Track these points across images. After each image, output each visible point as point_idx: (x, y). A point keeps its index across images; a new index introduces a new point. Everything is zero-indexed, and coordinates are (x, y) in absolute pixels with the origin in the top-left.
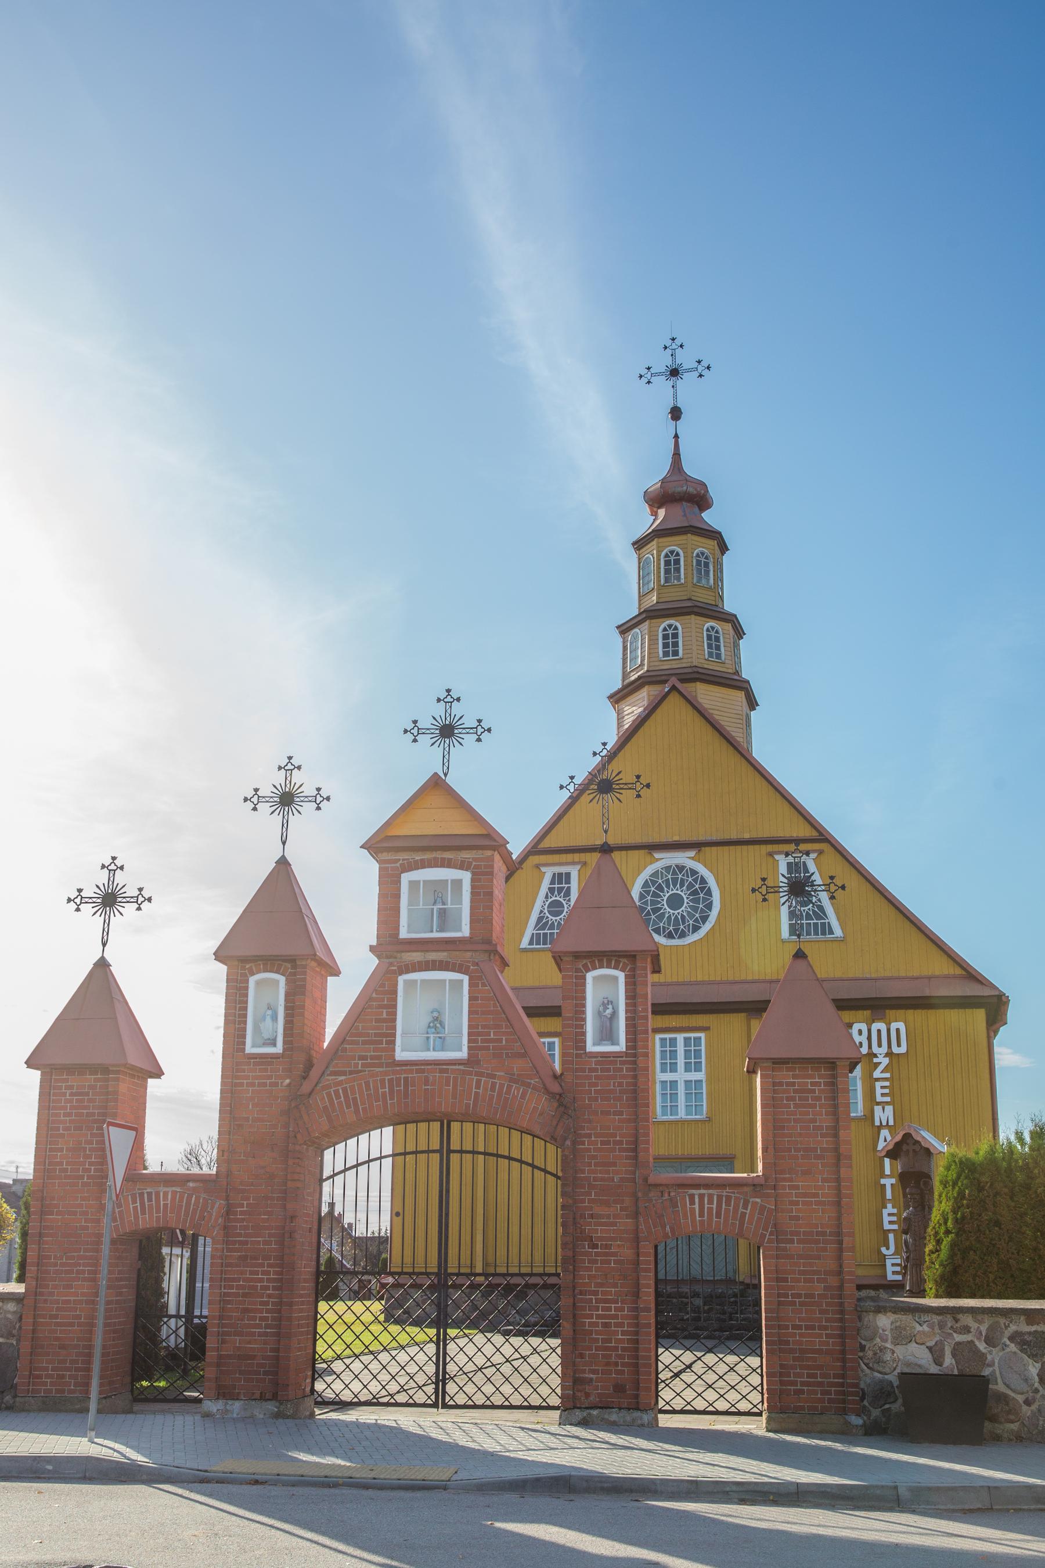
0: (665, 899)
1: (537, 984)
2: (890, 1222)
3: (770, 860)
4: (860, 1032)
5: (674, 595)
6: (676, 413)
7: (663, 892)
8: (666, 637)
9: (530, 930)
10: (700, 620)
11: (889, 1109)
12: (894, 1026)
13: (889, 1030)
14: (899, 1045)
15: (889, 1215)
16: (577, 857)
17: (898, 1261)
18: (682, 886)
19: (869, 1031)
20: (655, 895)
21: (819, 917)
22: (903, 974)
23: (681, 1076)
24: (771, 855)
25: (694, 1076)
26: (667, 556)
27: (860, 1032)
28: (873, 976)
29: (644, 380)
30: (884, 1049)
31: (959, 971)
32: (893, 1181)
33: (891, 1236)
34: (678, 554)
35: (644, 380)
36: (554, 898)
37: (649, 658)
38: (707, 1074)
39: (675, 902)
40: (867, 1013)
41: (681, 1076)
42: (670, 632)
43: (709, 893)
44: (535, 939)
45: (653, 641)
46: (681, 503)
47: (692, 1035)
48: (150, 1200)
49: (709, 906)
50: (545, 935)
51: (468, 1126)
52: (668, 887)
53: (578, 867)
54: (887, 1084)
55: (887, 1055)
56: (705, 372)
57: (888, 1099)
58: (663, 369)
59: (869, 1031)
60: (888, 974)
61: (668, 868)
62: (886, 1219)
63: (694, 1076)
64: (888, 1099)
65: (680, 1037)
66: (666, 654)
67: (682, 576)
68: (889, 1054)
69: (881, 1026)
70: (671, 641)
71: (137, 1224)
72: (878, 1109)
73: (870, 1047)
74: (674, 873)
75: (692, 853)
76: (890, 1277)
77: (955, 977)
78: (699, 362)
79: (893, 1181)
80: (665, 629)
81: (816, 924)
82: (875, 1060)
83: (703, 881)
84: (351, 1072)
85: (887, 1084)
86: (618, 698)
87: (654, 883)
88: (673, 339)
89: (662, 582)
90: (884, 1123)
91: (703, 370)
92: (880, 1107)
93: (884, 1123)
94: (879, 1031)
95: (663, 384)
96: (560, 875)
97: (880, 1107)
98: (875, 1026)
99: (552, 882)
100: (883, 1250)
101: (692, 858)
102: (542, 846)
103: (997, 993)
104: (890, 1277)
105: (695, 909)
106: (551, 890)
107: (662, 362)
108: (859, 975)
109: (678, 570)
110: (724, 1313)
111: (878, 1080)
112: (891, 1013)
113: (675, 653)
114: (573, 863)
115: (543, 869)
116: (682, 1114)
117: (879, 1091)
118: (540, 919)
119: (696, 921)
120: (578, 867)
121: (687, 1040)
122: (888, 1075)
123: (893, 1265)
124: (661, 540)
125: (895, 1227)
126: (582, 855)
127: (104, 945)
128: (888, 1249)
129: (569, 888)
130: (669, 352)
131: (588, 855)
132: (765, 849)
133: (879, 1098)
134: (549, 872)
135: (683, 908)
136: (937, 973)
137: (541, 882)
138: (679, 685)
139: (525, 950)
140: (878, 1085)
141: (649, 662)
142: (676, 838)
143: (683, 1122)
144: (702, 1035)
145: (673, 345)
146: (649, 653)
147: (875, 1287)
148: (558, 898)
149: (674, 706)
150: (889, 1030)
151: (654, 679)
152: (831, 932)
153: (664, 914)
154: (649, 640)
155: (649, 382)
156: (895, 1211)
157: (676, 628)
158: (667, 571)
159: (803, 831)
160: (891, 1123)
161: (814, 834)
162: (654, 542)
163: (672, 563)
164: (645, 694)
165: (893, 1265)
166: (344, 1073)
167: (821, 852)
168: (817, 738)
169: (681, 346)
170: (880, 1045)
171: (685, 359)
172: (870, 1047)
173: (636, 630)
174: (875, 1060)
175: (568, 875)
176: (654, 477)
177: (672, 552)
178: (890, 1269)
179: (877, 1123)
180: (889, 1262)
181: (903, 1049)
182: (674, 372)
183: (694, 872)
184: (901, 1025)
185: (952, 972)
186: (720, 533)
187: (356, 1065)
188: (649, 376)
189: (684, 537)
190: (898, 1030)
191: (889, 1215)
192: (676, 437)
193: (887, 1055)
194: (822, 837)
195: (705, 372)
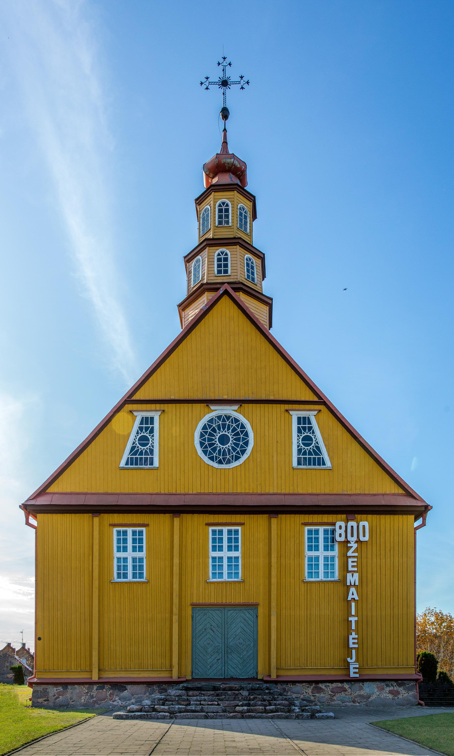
0: (217, 437)
1: (131, 491)
2: (354, 643)
3: (287, 414)
4: (340, 527)
6: (225, 114)
7: (216, 432)
8: (219, 260)
9: (126, 455)
11: (356, 575)
12: (361, 524)
13: (358, 527)
14: (364, 536)
15: (353, 639)
16: (158, 406)
17: (357, 666)
18: (220, 450)
19: (346, 527)
20: (210, 434)
21: (316, 454)
22: (367, 492)
23: (225, 554)
25: (233, 554)
26: (220, 206)
27: (340, 527)
28: (349, 493)
29: (204, 86)
30: (355, 538)
31: (401, 491)
32: (356, 619)
33: (354, 651)
34: (227, 205)
35: (204, 86)
36: (142, 434)
37: (208, 274)
38: (242, 553)
39: (224, 440)
40: (344, 516)
41: (225, 554)
43: (247, 434)
45: (210, 263)
47: (233, 528)
49: (247, 444)
50: (136, 459)
52: (219, 429)
53: (160, 413)
54: (356, 560)
55: (356, 542)
56: (245, 86)
57: (355, 569)
58: (217, 80)
59: (346, 527)
60: (358, 492)
61: (219, 417)
62: (351, 641)
63: (233, 554)
64: (355, 569)
65: (225, 529)
66: (219, 272)
67: (230, 221)
68: (358, 541)
69: (354, 524)
70: (223, 263)
72: (349, 575)
73: (346, 537)
75: (236, 407)
76: (352, 675)
77: (399, 495)
78: (242, 77)
79: (356, 619)
80: (219, 255)
81: (314, 459)
82: (349, 545)
83: (243, 427)
85: (356, 560)
86: (184, 306)
87: (210, 426)
88: (224, 58)
89: (217, 224)
90: (353, 584)
91: (243, 83)
92: (351, 574)
93: (353, 584)
94: (352, 527)
95: (216, 90)
96: (147, 418)
97: (351, 574)
98: (351, 523)
99: (141, 423)
100: (349, 659)
101: (235, 411)
102: (134, 398)
103: (424, 504)
104: (352, 675)
105: (234, 449)
106: (141, 429)
107: (216, 75)
108: (340, 492)
109: (227, 216)
110: (264, 700)
111: (350, 557)
112: (358, 517)
113: (226, 272)
114: (156, 411)
115: (135, 414)
116: (225, 578)
117: (350, 564)
118: (133, 448)
120: (160, 413)
121: (230, 532)
122: (356, 554)
123: (354, 668)
124: (217, 194)
125: (356, 646)
126: (162, 405)
128: (351, 659)
129: (153, 428)
130: (221, 67)
131: (166, 405)
133: (350, 569)
134: (139, 416)
135: (229, 444)
136: (388, 492)
137: (134, 422)
139: (123, 469)
140: (350, 560)
141: (208, 277)
143: (226, 582)
144: (239, 528)
145: (224, 63)
146: (208, 271)
147: (342, 681)
148: (145, 434)
149: (225, 299)
150: (358, 527)
152: (324, 464)
153: (216, 447)
154: (208, 262)
155: (207, 88)
156: (357, 636)
157: (226, 254)
158: (220, 217)
160: (357, 583)
162: (212, 196)
163: (223, 212)
164: (205, 298)
165: (354, 668)
168: (329, 322)
169: (230, 64)
170: (352, 536)
171: (233, 74)
172: (346, 537)
173: (199, 257)
174: (349, 545)
175: (152, 419)
177: (223, 203)
178: (352, 670)
179: (348, 584)
180: (351, 667)
181: (367, 538)
182: (225, 83)
183: (237, 420)
184: (366, 524)
185: (397, 492)
186: (254, 197)
189: (232, 193)
190: (364, 526)
191: (353, 639)
192: (225, 130)
193: (356, 542)
194: (321, 401)
195: (245, 86)
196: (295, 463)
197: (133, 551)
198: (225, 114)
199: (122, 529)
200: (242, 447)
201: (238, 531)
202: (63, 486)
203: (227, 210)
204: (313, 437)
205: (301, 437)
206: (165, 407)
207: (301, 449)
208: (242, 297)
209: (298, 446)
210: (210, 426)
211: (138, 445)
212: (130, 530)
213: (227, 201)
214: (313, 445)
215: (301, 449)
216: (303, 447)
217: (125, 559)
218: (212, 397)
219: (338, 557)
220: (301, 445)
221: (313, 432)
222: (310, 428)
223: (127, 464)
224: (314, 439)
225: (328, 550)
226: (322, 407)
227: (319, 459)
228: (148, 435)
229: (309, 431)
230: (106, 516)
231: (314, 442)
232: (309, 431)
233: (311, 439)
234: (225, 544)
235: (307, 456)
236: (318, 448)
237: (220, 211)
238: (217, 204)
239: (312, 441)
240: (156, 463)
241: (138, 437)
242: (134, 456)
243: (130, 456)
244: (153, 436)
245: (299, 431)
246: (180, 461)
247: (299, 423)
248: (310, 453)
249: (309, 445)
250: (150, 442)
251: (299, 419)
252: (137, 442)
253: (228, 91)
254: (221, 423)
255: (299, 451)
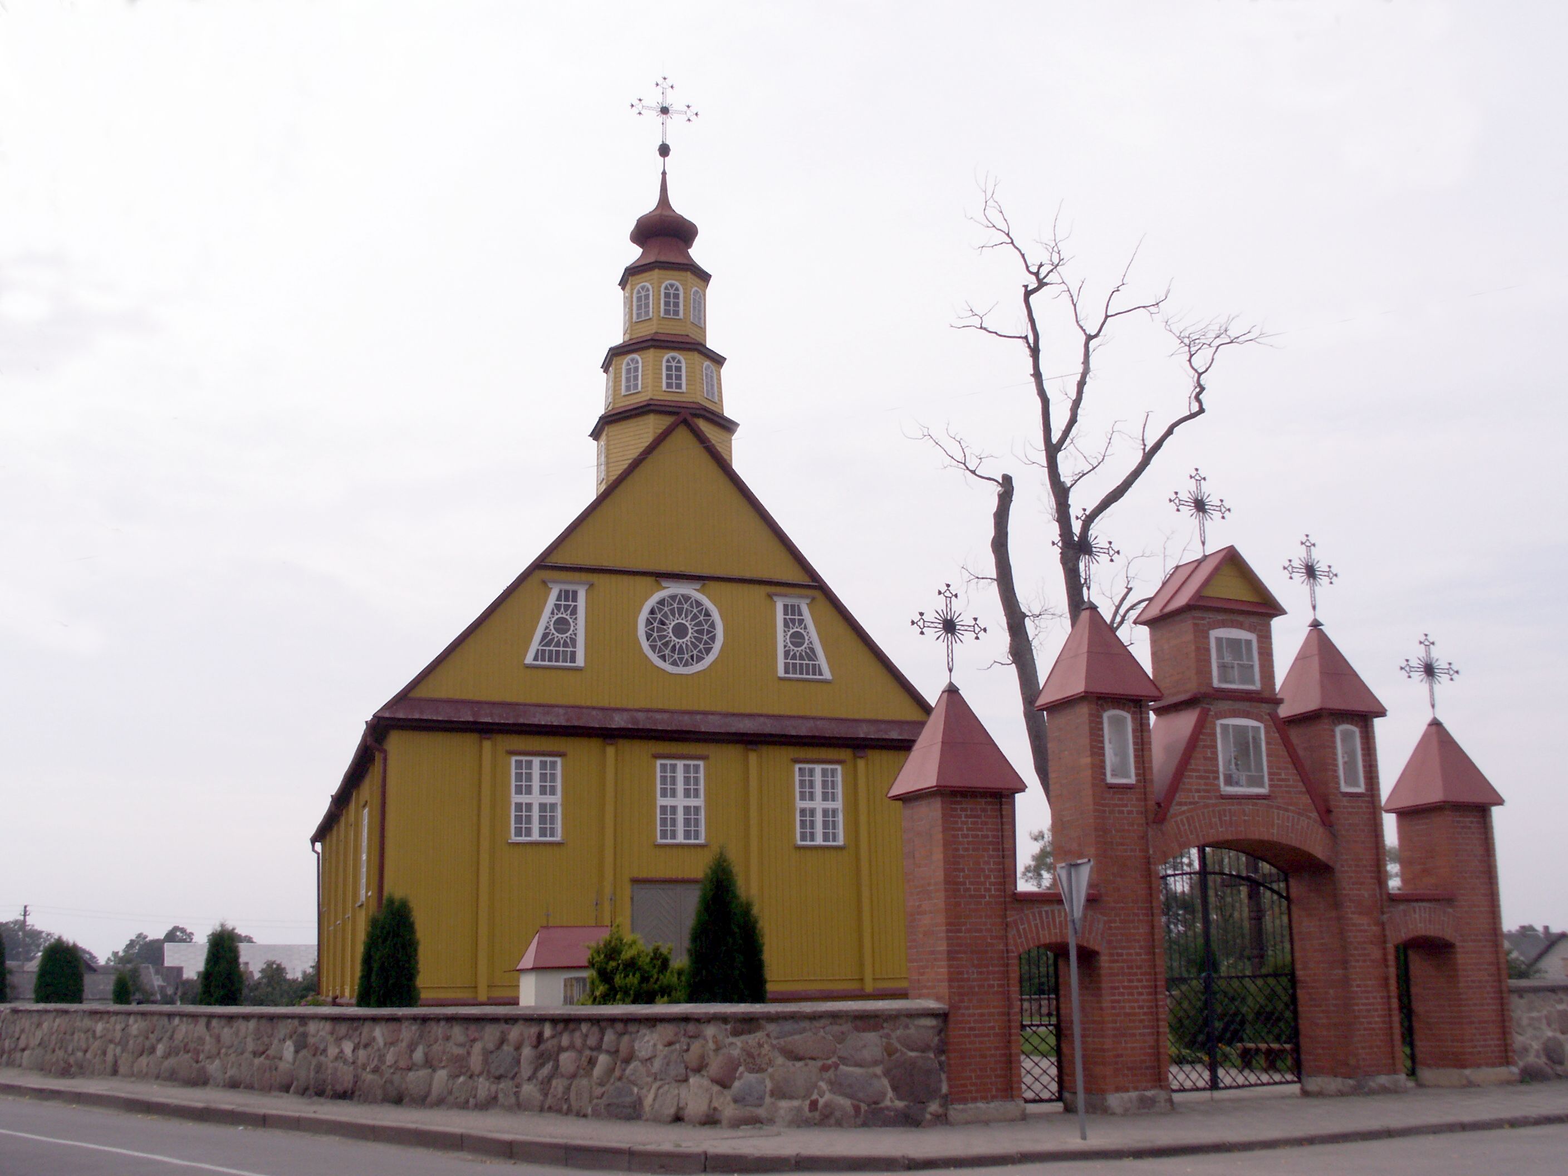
5: (646, 331)
6: (664, 150)
9: (535, 645)
10: (659, 352)
16: (584, 576)
23: (680, 802)
24: (770, 596)
36: (560, 615)
38: (705, 801)
39: (680, 631)
41: (680, 802)
42: (674, 364)
44: (539, 655)
46: (664, 238)
48: (1047, 917)
50: (551, 651)
51: (1232, 853)
70: (674, 373)
71: (1039, 939)
74: (680, 603)
84: (1191, 803)
89: (662, 314)
96: (567, 592)
99: (559, 599)
106: (558, 607)
113: (679, 386)
118: (545, 636)
119: (700, 651)
127: (951, 670)
130: (659, 89)
132: (762, 590)
138: (689, 418)
142: (682, 569)
149: (682, 437)
151: (663, 409)
157: (679, 362)
158: (667, 304)
159: (800, 578)
161: (805, 580)
166: (1185, 804)
167: (813, 599)
176: (648, 204)
177: (672, 286)
183: (699, 604)
187: (1193, 797)
188: (640, 107)
192: (664, 174)
194: (815, 585)
196: (781, 673)
197: (541, 794)
198: (664, 150)
199: (668, 762)
200: (706, 643)
201: (1112, 775)
202: (441, 689)
203: (676, 296)
204: (805, 634)
205: (789, 634)
206: (594, 578)
207: (789, 651)
208: (703, 426)
209: (785, 646)
210: (660, 610)
211: (553, 631)
212: (536, 761)
213: (677, 283)
214: (805, 645)
215: (789, 651)
216: (792, 647)
217: (529, 806)
218: (663, 568)
219: (562, 805)
220: (789, 644)
221: (805, 628)
222: (801, 621)
223: (536, 659)
224: (807, 638)
225: (545, 794)
226: (817, 593)
227: (814, 666)
228: (568, 617)
229: (800, 625)
230: (499, 738)
231: (807, 642)
232: (800, 625)
233: (802, 636)
234: (680, 787)
235: (798, 662)
236: (812, 650)
237: (667, 295)
238: (663, 286)
239: (804, 638)
240: (580, 661)
241: (553, 620)
242: (547, 648)
243: (540, 648)
244: (576, 619)
245: (786, 625)
246: (585, 656)
247: (786, 613)
248: (801, 658)
249: (801, 644)
250: (572, 628)
251: (786, 606)
252: (552, 627)
253: (669, 121)
254: (675, 605)
255: (787, 654)
